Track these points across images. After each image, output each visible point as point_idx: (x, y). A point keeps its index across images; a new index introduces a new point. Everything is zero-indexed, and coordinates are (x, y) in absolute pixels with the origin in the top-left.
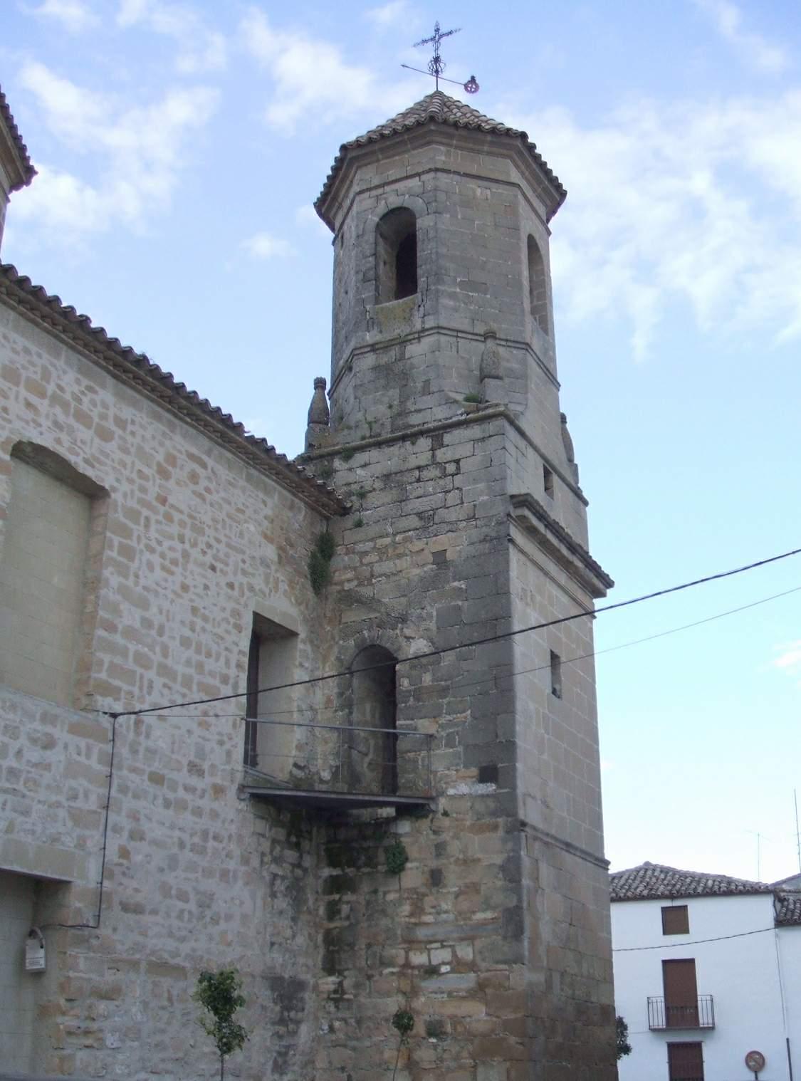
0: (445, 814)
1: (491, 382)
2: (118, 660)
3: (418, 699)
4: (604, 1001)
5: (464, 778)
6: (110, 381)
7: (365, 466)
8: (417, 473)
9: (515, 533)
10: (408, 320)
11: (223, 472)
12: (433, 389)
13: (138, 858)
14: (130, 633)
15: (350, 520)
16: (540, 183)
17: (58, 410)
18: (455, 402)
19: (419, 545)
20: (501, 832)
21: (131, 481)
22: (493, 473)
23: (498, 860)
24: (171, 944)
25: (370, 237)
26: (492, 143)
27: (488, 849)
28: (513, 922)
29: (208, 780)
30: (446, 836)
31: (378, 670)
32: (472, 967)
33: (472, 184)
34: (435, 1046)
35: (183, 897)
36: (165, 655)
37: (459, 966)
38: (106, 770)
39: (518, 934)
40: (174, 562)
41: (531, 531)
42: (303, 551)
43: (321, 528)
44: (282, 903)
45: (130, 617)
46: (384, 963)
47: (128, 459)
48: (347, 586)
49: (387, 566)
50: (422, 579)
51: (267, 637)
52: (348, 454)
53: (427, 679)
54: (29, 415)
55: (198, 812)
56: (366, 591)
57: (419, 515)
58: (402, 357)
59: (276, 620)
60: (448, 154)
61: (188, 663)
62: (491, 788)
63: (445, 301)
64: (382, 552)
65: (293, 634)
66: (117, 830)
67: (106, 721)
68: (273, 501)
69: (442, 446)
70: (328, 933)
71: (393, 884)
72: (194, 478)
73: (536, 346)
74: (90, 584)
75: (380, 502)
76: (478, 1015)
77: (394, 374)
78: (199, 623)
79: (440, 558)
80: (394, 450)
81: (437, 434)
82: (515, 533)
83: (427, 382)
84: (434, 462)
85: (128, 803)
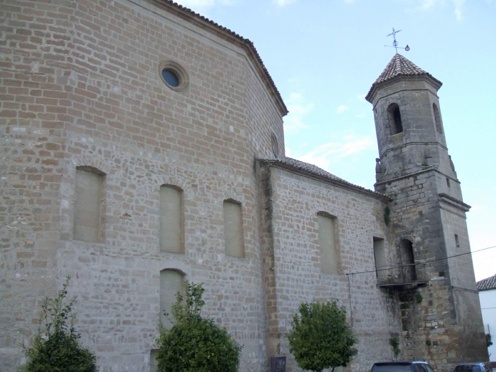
0: (431, 286)
1: (428, 159)
2: (346, 260)
3: (420, 254)
4: (482, 331)
5: (435, 275)
6: (332, 187)
7: (395, 186)
8: (411, 188)
9: (441, 204)
10: (402, 140)
11: (360, 201)
12: (412, 162)
13: (357, 308)
14: (348, 252)
15: (393, 203)
16: (434, 83)
17: (324, 200)
18: (419, 166)
19: (414, 210)
20: (447, 290)
21: (341, 212)
22: (433, 188)
23: (447, 297)
24: (367, 328)
25: (386, 113)
26: (418, 78)
27: (444, 294)
28: (453, 314)
29: (369, 285)
30: (432, 292)
31: (407, 246)
32: (443, 326)
33: (414, 93)
34: (436, 348)
35: (368, 316)
36: (355, 255)
37: (440, 326)
38: (348, 288)
39: (455, 317)
40: (354, 230)
41: (445, 202)
42: (382, 214)
43: (385, 206)
44: (390, 313)
45: (347, 248)
46: (419, 327)
47: (340, 206)
48: (395, 222)
49: (406, 216)
50: (416, 220)
51: (377, 241)
52: (389, 183)
53: (421, 248)
54: (318, 204)
55: (368, 294)
56: (401, 224)
57: (413, 201)
58: (401, 152)
59: (378, 237)
60: (405, 84)
61: (361, 255)
62: (443, 278)
63: (412, 134)
64: (404, 212)
65: (382, 239)
66: (353, 302)
67: (346, 276)
68: (373, 203)
69: (417, 180)
70: (403, 320)
71: (419, 305)
72: (354, 205)
73: (440, 142)
74: (336, 242)
75: (401, 198)
76: (446, 339)
77: (399, 158)
78: (361, 244)
79: (420, 213)
80: (403, 181)
81: (415, 176)
82: (441, 204)
83: (410, 160)
84: (415, 185)
85: (354, 295)
